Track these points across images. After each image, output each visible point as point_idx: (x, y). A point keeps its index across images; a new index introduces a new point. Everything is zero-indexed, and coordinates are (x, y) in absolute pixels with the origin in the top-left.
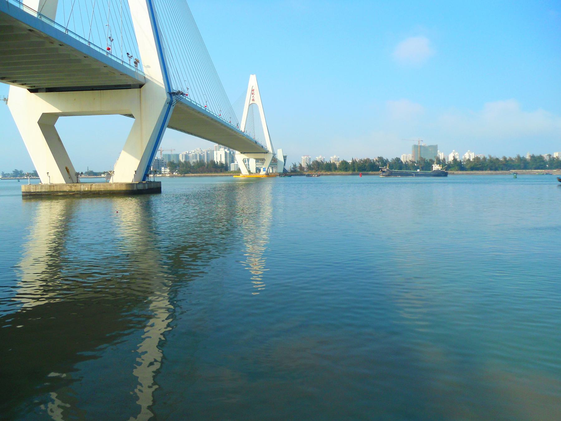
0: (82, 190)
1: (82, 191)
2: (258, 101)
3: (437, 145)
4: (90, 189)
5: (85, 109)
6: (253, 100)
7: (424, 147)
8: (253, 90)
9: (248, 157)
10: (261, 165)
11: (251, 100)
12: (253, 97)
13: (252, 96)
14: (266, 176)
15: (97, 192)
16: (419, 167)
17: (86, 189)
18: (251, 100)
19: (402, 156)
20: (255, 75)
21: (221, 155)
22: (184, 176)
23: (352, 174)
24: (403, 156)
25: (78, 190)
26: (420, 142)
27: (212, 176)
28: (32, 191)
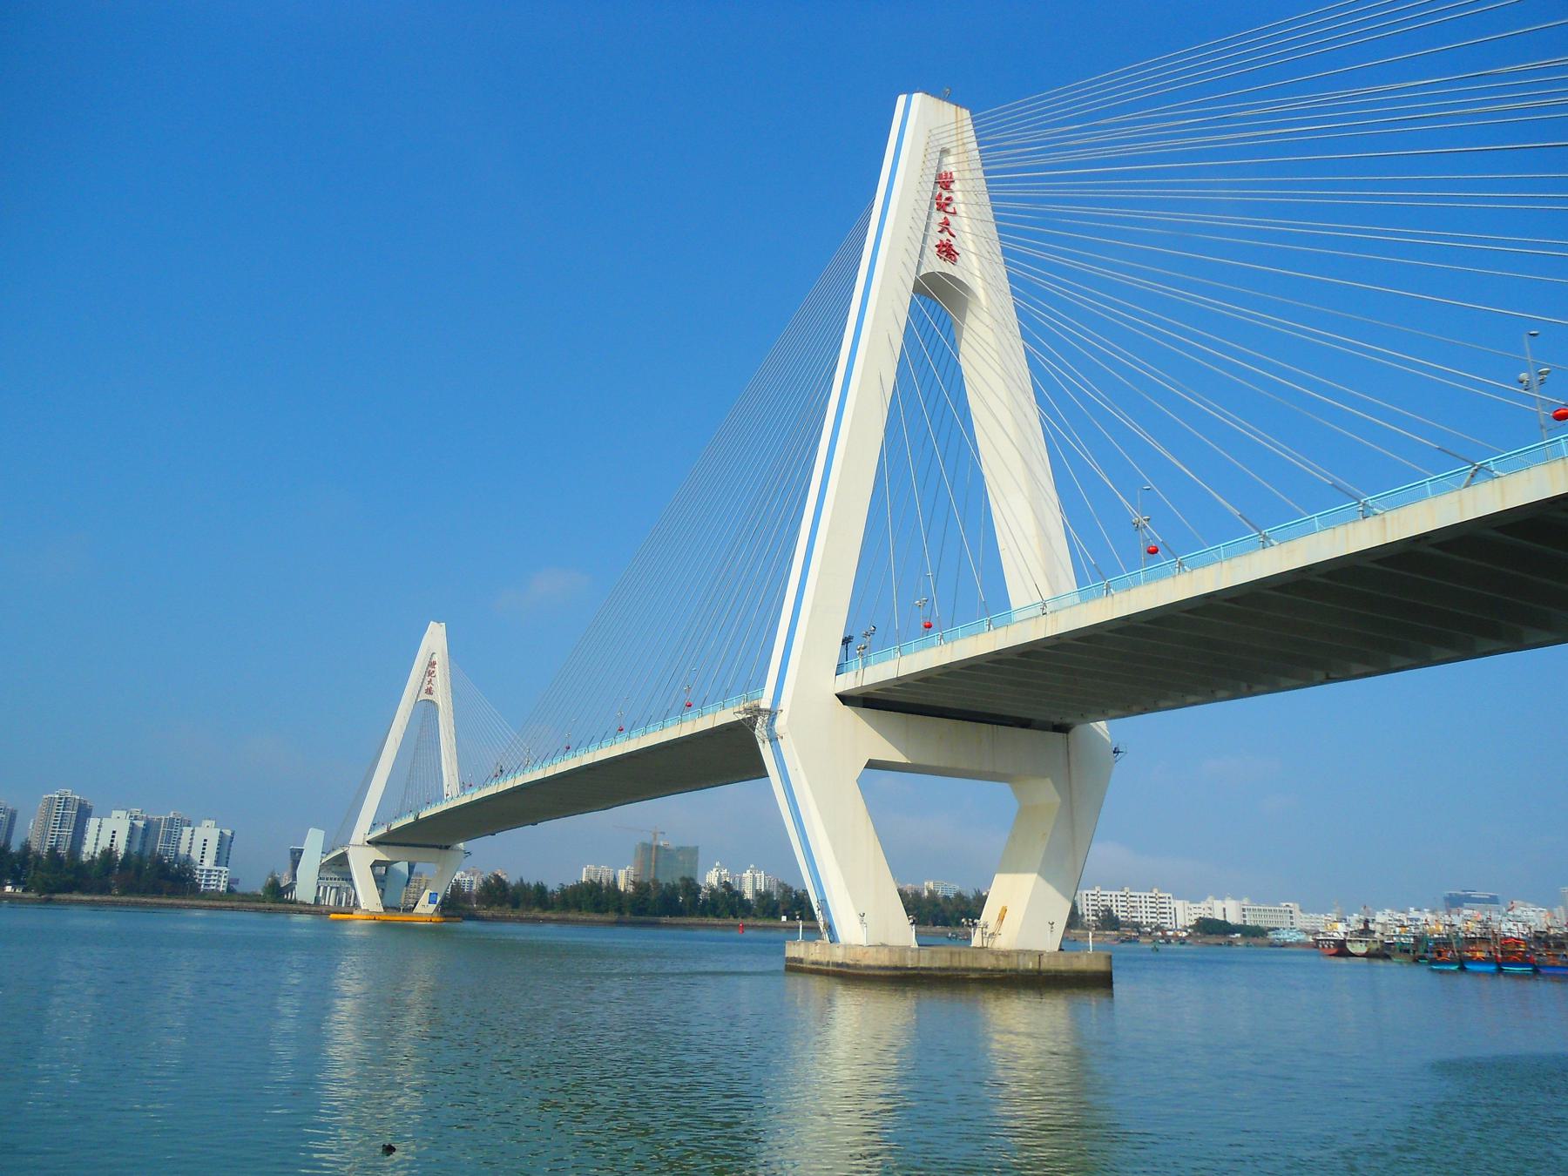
0: (1021, 968)
1: (1022, 971)
2: (442, 697)
3: (697, 847)
4: (1037, 967)
5: (963, 765)
6: (429, 691)
7: (665, 849)
8: (432, 664)
9: (387, 856)
10: (335, 879)
11: (423, 691)
12: (430, 682)
13: (428, 679)
14: (442, 919)
15: (1053, 973)
16: (1075, 927)
17: (1030, 966)
18: (423, 691)
19: (584, 869)
20: (443, 624)
21: (114, 832)
22: (48, 901)
23: (618, 923)
24: (588, 872)
25: (1014, 967)
26: (658, 835)
27: (686, 926)
28: (909, 966)
